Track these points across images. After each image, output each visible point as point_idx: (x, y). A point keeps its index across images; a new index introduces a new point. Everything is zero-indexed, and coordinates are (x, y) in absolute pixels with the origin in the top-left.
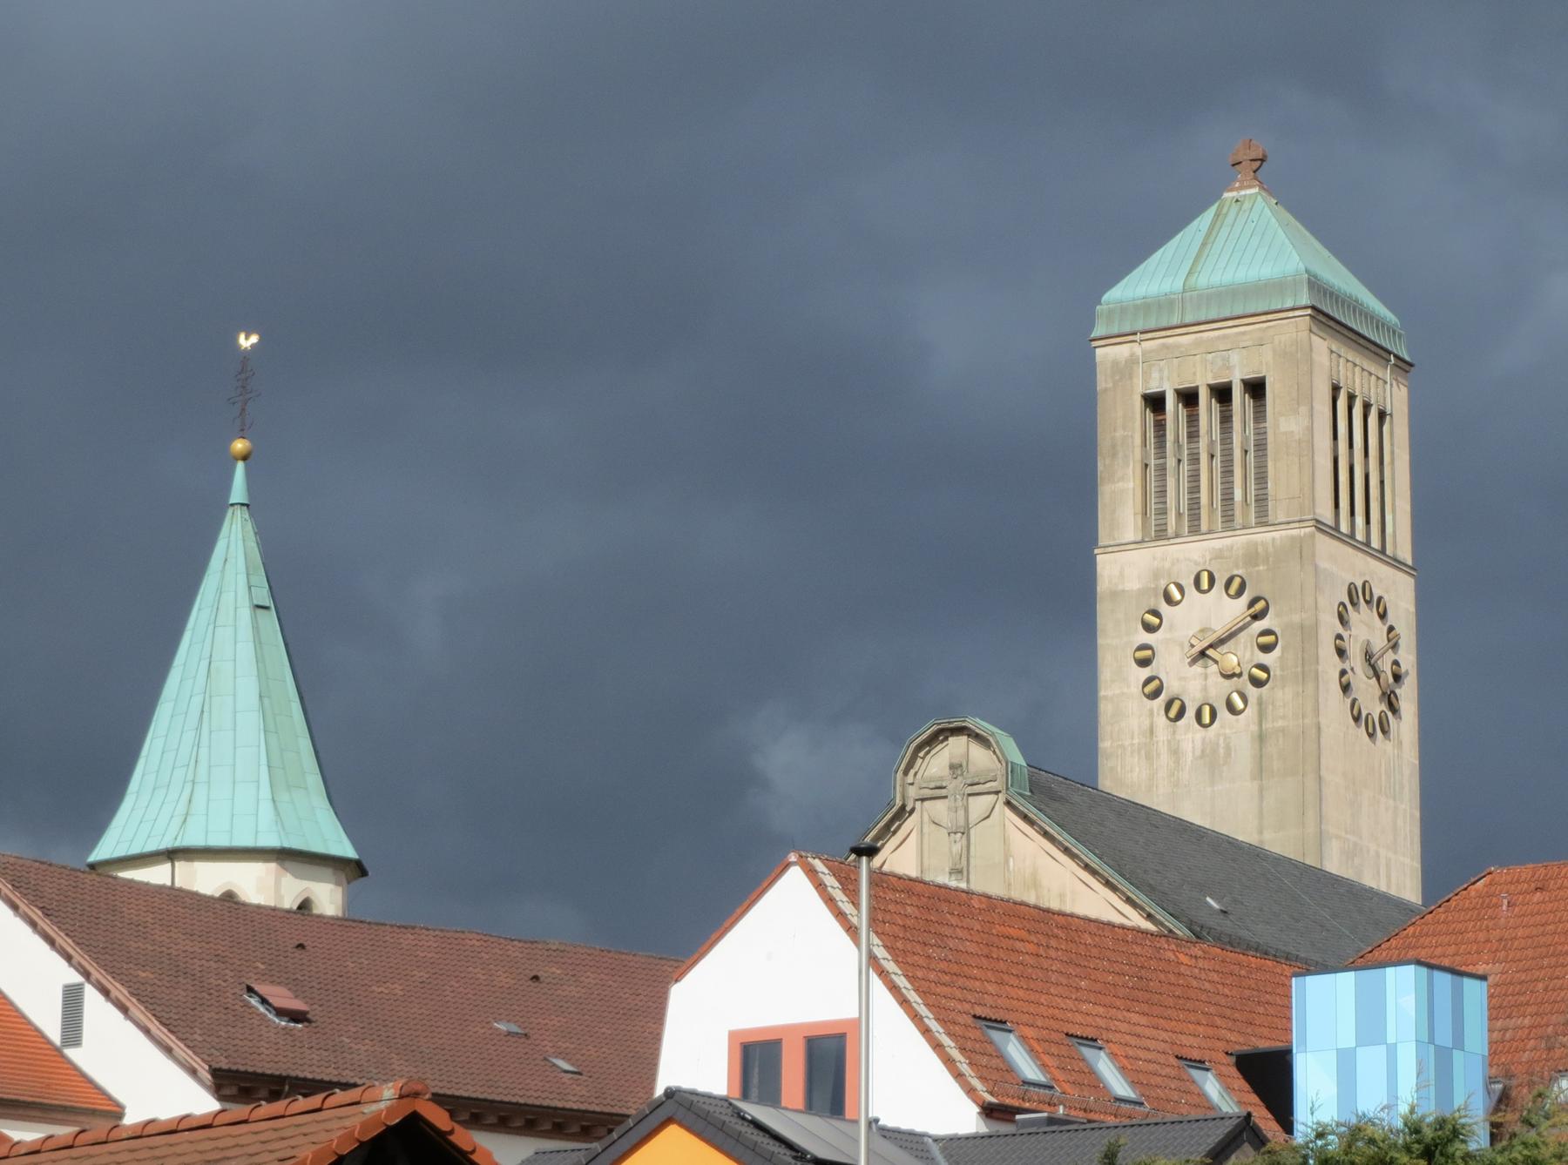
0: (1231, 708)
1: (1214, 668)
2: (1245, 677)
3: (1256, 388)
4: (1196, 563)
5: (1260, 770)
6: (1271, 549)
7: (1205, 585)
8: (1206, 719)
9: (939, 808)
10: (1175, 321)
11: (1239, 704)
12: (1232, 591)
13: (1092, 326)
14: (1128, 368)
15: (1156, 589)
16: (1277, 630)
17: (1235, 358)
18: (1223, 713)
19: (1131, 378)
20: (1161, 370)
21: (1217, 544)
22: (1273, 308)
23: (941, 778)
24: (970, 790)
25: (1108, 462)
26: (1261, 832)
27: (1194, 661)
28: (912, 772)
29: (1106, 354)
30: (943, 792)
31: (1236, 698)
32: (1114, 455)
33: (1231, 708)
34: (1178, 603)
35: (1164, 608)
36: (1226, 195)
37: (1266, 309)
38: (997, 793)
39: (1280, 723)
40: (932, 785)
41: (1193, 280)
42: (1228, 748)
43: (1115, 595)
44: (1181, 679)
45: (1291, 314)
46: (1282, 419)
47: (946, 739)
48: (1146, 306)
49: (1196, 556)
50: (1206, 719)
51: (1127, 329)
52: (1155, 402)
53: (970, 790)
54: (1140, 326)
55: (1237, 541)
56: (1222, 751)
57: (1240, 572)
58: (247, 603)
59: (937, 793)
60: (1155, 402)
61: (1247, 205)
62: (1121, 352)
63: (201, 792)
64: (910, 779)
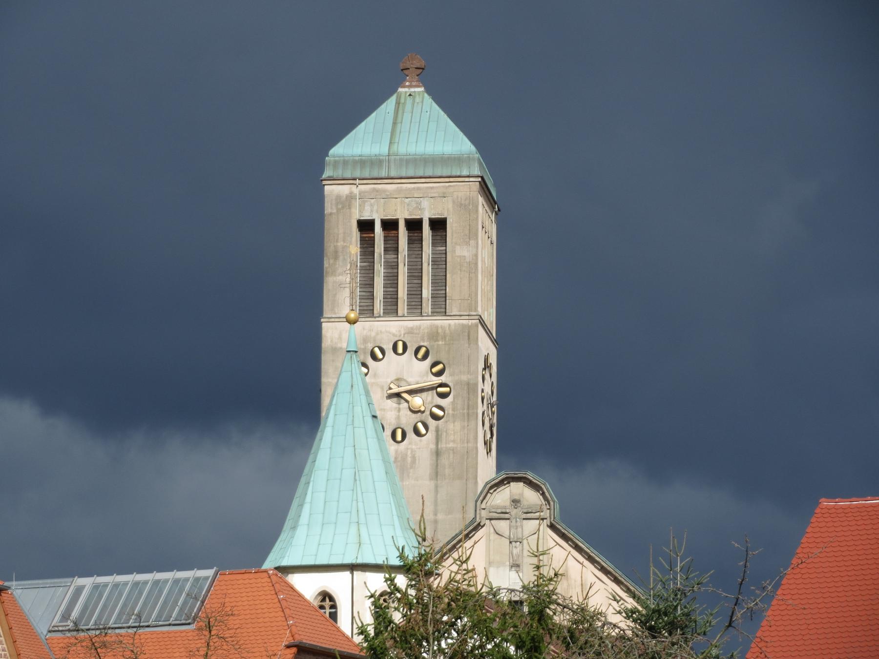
0: (417, 432)
1: (405, 405)
2: (428, 413)
3: (439, 225)
4: (394, 335)
5: (436, 474)
6: (447, 331)
7: (400, 350)
8: (399, 438)
9: (503, 526)
10: (383, 174)
11: (422, 430)
12: (420, 355)
13: (322, 172)
14: (347, 201)
15: (365, 348)
16: (450, 384)
17: (425, 203)
18: (411, 435)
19: (350, 208)
20: (372, 205)
21: (410, 324)
22: (454, 174)
23: (505, 507)
24: (525, 516)
25: (331, 261)
26: (436, 515)
27: (390, 396)
28: (485, 501)
29: (331, 190)
30: (507, 516)
31: (420, 426)
32: (336, 258)
33: (417, 432)
34: (381, 360)
35: (370, 362)
36: (400, 90)
37: (449, 174)
38: (543, 519)
39: (451, 445)
40: (499, 511)
41: (395, 148)
42: (414, 457)
43: (335, 350)
44: (381, 410)
45: (467, 179)
46: (458, 247)
47: (509, 483)
48: (362, 162)
49: (394, 331)
50: (399, 438)
51: (349, 175)
52: (366, 226)
53: (525, 516)
54: (358, 174)
55: (424, 324)
56: (409, 459)
57: (425, 344)
58: (370, 415)
59: (502, 515)
60: (366, 226)
61: (418, 99)
62: (344, 190)
63: (363, 529)
64: (483, 506)
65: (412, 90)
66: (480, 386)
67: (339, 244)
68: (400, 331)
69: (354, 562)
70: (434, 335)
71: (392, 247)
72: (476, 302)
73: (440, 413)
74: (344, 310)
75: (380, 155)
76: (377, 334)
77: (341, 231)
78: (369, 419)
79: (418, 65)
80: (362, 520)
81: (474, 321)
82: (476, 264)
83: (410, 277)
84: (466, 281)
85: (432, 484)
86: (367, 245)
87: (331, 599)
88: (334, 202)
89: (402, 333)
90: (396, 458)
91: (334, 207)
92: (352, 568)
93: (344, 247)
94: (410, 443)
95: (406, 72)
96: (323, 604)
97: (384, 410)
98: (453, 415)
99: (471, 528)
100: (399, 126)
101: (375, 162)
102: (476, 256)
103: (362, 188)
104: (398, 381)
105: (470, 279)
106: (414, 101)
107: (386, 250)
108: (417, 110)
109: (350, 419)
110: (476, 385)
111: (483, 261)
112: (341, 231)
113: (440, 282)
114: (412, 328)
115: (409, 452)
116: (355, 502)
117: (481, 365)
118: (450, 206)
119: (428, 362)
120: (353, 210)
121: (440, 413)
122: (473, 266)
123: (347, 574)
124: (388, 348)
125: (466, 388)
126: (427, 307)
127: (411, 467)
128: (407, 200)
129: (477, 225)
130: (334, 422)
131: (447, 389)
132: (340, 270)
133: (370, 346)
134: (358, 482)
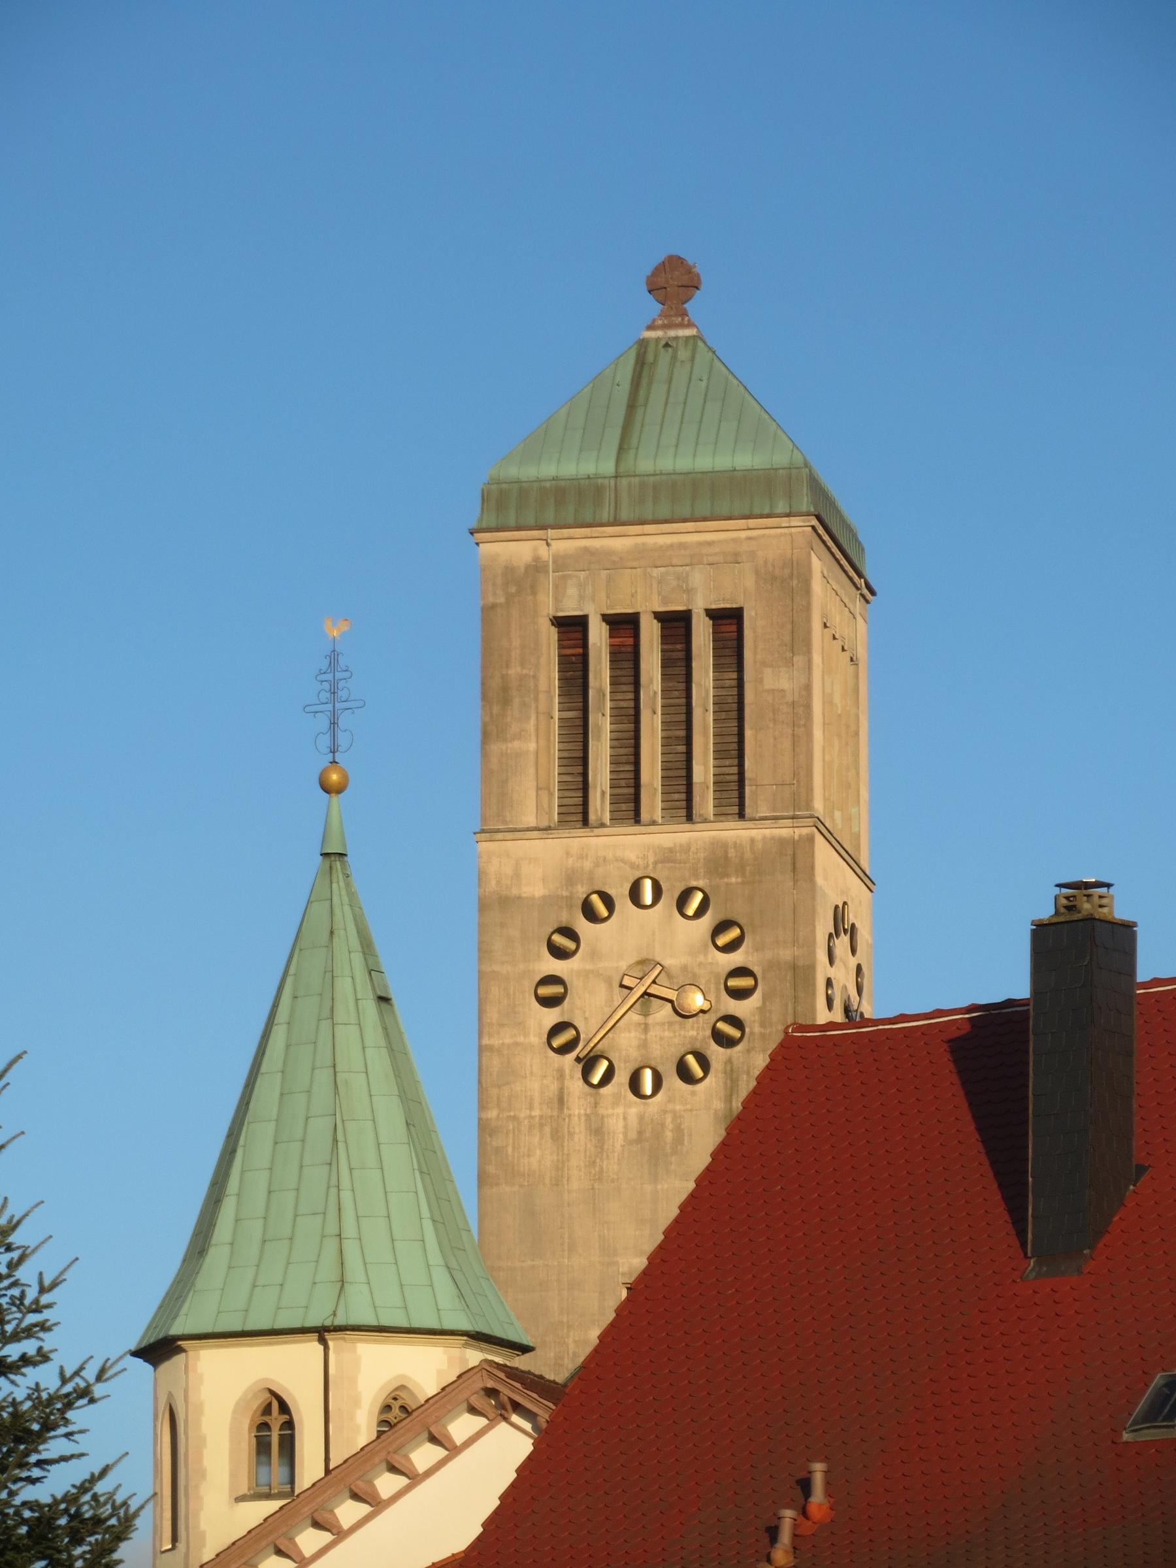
3: (728, 620)
4: (633, 866)
6: (748, 855)
15: (570, 898)
16: (756, 969)
17: (697, 578)
42: (678, 1130)
46: (768, 672)
49: (632, 856)
52: (572, 628)
56: (669, 1135)
57: (700, 883)
60: (572, 628)
65: (672, 333)
66: (823, 970)
67: (512, 672)
68: (644, 857)
70: (719, 861)
72: (810, 790)
75: (597, 476)
76: (597, 865)
77: (516, 643)
78: (370, 1007)
80: (350, 1229)
81: (805, 831)
82: (808, 707)
84: (786, 744)
87: (284, 1408)
88: (499, 581)
89: (651, 860)
91: (500, 592)
93: (522, 678)
94: (671, 1100)
96: (266, 1419)
102: (808, 688)
103: (560, 546)
104: (645, 964)
105: (795, 740)
106: (674, 358)
109: (328, 1003)
110: (812, 968)
111: (828, 701)
112: (516, 643)
113: (733, 748)
114: (671, 850)
115: (669, 1119)
116: (333, 1191)
117: (824, 926)
118: (750, 582)
119: (706, 922)
120: (541, 597)
122: (800, 710)
124: (620, 893)
126: (705, 801)
127: (674, 1152)
128: (656, 572)
129: (808, 620)
130: (291, 1015)
132: (514, 728)
133: (581, 891)
134: (341, 1145)
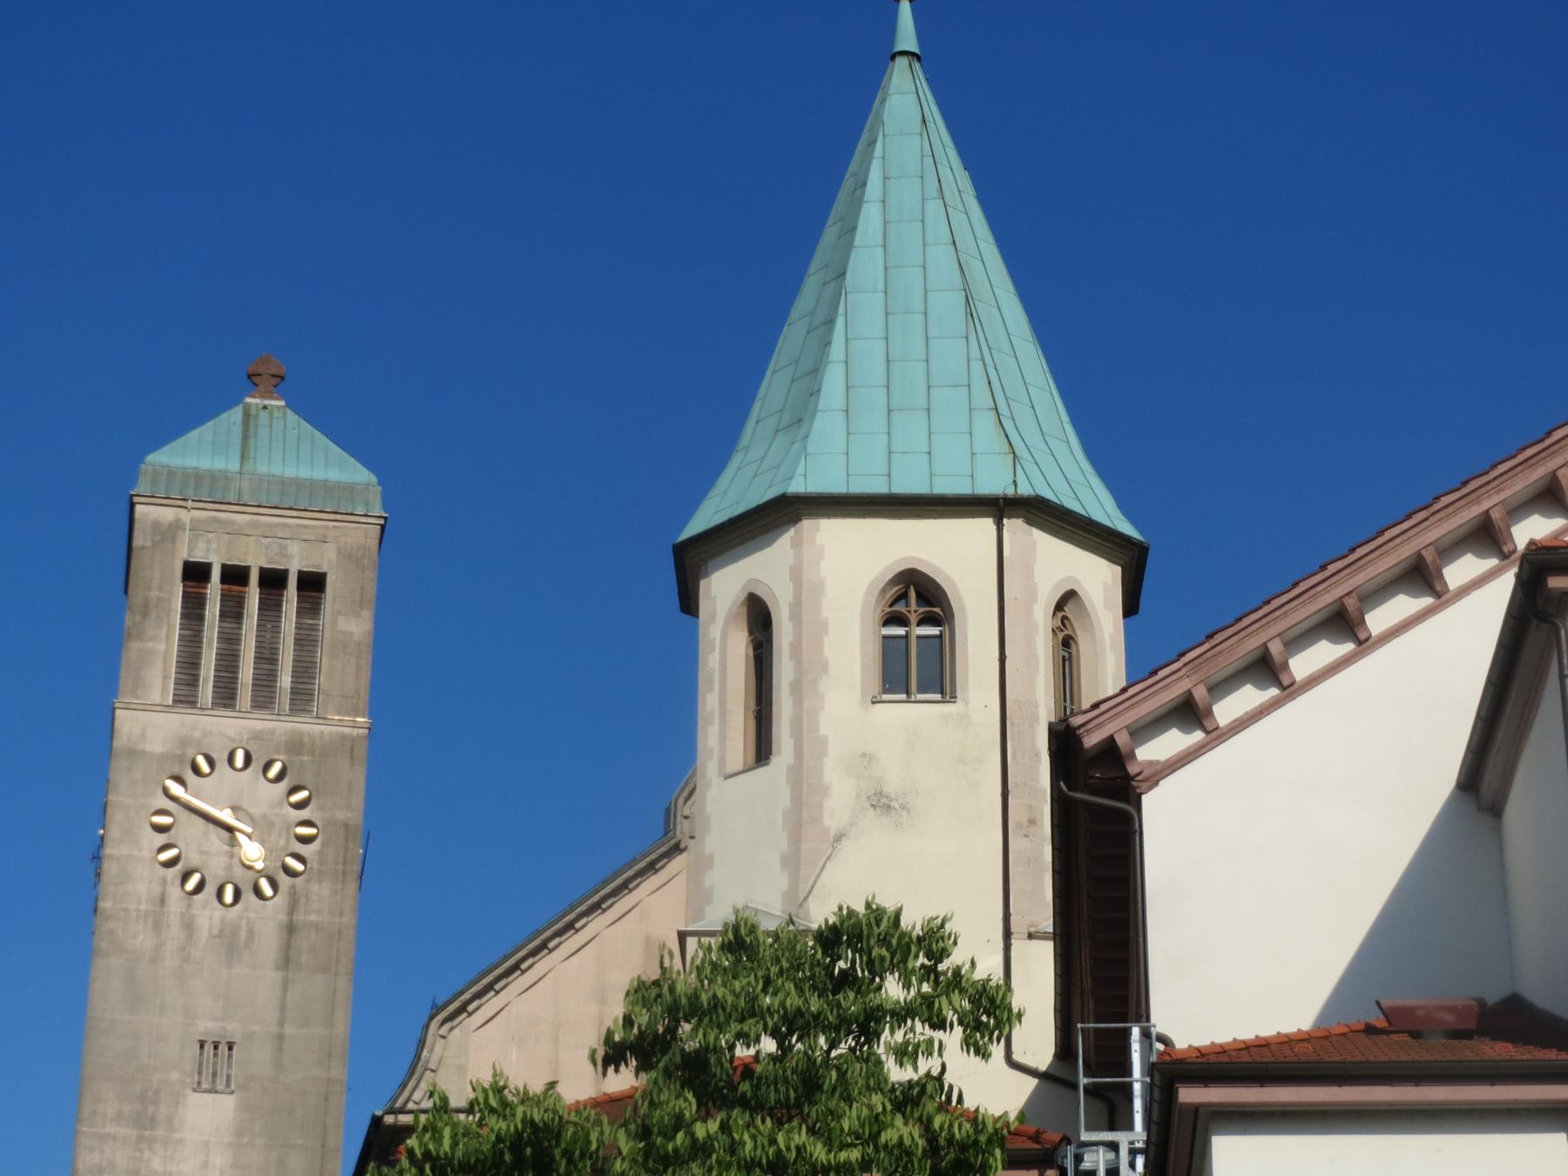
3: (312, 584)
4: (231, 740)
5: (286, 961)
14: (175, 530)
17: (294, 548)
20: (209, 542)
21: (258, 725)
32: (145, 611)
39: (313, 918)
41: (249, 466)
43: (133, 753)
46: (341, 619)
48: (198, 477)
49: (231, 733)
52: (195, 573)
55: (280, 725)
56: (243, 935)
60: (195, 573)
61: (277, 414)
62: (167, 514)
69: (1010, 492)
71: (233, 611)
73: (299, 867)
74: (155, 697)
79: (275, 371)
83: (259, 658)
85: (279, 976)
86: (193, 608)
90: (222, 930)
92: (999, 507)
93: (159, 599)
94: (246, 910)
95: (255, 379)
97: (207, 853)
98: (320, 872)
99: (607, 890)
100: (252, 441)
101: (215, 478)
107: (223, 615)
108: (278, 425)
115: (244, 923)
118: (333, 556)
121: (299, 867)
123: (983, 527)
124: (221, 757)
125: (342, 831)
126: (284, 699)
128: (265, 541)
131: (312, 831)
